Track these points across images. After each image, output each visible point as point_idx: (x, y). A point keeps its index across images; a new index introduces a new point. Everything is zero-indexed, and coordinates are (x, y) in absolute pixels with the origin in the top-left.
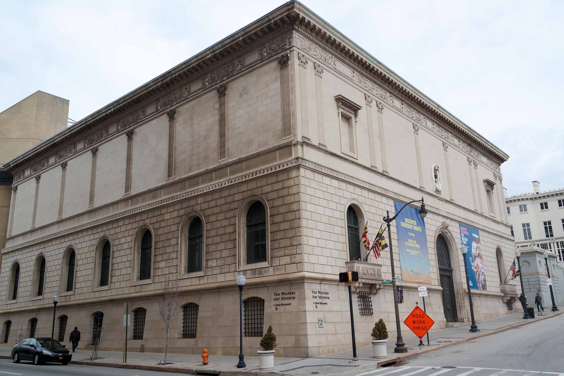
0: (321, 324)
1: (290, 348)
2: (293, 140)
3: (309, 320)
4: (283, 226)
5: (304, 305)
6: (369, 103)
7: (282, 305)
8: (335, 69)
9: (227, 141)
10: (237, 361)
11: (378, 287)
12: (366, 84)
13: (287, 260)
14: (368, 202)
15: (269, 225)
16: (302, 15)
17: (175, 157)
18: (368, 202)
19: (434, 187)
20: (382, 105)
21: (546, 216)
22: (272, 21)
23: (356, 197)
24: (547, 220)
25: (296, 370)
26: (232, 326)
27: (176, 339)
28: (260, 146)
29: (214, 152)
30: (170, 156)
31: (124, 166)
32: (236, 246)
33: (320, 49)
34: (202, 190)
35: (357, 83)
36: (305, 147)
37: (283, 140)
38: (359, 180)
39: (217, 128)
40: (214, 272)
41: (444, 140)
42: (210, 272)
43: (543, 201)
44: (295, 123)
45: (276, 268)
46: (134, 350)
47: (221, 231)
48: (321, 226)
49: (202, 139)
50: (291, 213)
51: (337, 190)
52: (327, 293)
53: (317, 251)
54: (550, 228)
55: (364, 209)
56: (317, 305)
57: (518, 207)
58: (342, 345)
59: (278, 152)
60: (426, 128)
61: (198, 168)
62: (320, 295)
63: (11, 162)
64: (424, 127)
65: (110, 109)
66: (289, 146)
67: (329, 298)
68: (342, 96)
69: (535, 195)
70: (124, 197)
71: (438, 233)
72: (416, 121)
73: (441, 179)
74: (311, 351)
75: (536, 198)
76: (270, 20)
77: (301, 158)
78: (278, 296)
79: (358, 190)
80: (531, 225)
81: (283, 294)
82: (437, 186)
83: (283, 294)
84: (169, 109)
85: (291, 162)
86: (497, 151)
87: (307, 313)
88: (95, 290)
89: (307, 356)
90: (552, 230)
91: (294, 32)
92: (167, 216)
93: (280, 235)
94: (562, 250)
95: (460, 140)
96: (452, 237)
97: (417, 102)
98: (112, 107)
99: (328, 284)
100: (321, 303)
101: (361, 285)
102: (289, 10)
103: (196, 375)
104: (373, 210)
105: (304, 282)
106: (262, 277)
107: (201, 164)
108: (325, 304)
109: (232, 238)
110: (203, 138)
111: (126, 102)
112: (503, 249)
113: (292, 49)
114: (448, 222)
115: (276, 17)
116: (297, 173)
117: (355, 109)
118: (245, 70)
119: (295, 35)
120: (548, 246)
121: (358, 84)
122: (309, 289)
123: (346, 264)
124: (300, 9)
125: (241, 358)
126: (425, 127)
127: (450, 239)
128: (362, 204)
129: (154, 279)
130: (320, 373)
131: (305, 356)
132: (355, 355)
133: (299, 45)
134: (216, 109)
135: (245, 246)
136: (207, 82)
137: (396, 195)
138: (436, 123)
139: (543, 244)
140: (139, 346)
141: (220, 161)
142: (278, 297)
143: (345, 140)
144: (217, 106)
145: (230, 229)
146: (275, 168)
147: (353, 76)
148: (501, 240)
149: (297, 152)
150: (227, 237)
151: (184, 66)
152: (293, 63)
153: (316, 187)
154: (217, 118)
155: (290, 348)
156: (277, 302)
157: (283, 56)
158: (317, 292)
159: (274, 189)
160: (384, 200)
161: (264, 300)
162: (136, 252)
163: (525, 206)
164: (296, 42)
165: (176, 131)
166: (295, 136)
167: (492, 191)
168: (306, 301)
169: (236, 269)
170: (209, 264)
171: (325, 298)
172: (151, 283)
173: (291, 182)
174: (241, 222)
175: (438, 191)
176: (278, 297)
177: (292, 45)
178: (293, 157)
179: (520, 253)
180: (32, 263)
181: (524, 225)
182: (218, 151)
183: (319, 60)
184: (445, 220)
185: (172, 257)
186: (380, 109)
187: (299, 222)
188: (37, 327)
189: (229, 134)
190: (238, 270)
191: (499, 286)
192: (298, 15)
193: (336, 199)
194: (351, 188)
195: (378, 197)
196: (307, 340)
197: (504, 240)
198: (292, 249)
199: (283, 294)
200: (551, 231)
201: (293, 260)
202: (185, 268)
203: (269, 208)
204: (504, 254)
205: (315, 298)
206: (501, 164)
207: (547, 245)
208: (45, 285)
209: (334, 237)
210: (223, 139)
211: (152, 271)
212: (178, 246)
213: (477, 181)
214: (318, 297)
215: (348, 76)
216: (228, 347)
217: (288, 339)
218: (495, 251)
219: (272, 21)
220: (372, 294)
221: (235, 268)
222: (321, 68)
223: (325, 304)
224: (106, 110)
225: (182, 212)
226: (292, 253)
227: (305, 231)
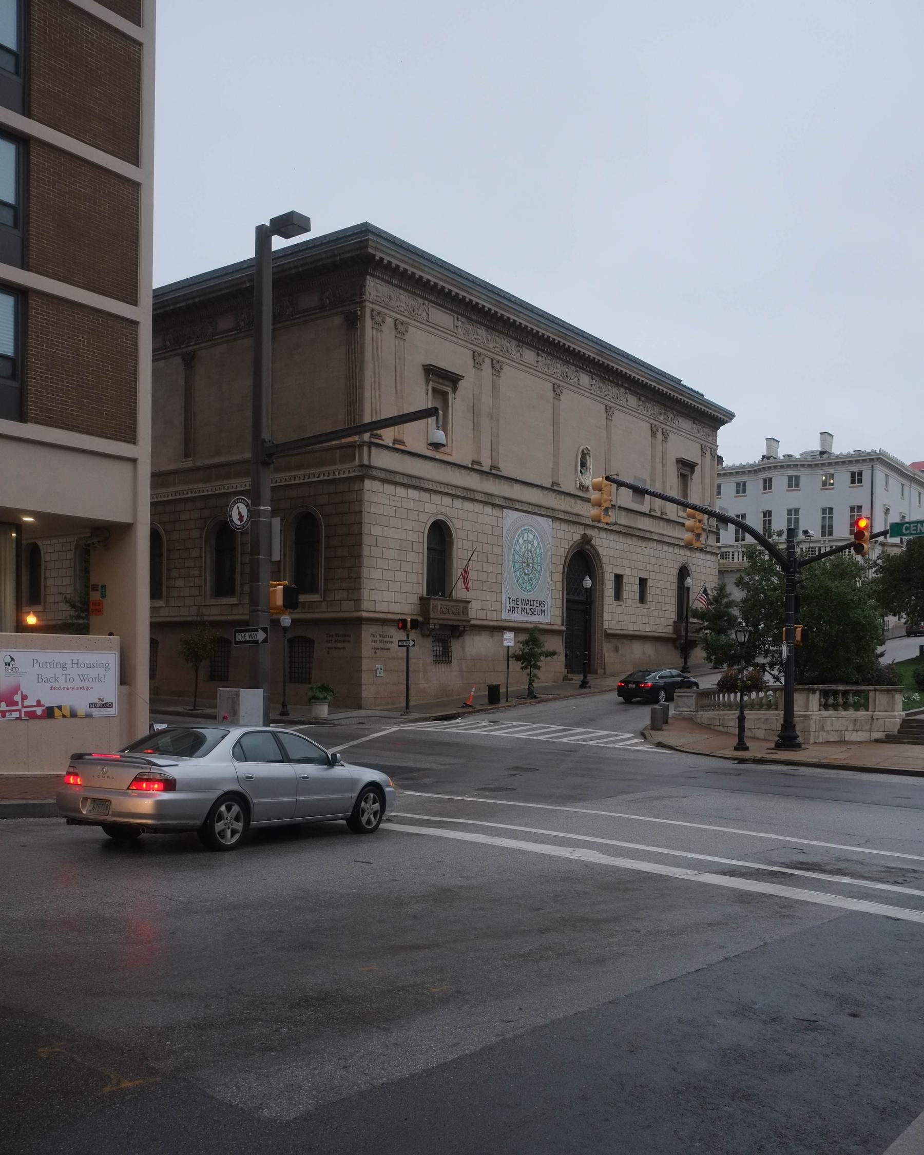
7: (335, 648)
11: (461, 629)
12: (477, 334)
13: (342, 595)
19: (578, 482)
23: (444, 510)
33: (406, 294)
34: (234, 486)
36: (373, 449)
57: (787, 478)
59: (338, 451)
62: (381, 639)
73: (591, 467)
80: (801, 512)
82: (582, 480)
83: (336, 636)
89: (360, 707)
91: (368, 277)
92: (184, 517)
100: (382, 649)
101: (437, 627)
105: (361, 624)
115: (343, 253)
117: (454, 380)
119: (370, 282)
122: (368, 634)
124: (376, 248)
125: (284, 705)
133: (375, 297)
136: (243, 320)
137: (507, 502)
138: (597, 375)
146: (334, 474)
147: (457, 327)
153: (386, 502)
158: (378, 636)
161: (313, 641)
167: (691, 476)
171: (388, 642)
172: (164, 606)
175: (583, 486)
176: (330, 639)
186: (496, 369)
192: (374, 256)
199: (337, 635)
213: (664, 462)
214: (378, 642)
219: (338, 258)
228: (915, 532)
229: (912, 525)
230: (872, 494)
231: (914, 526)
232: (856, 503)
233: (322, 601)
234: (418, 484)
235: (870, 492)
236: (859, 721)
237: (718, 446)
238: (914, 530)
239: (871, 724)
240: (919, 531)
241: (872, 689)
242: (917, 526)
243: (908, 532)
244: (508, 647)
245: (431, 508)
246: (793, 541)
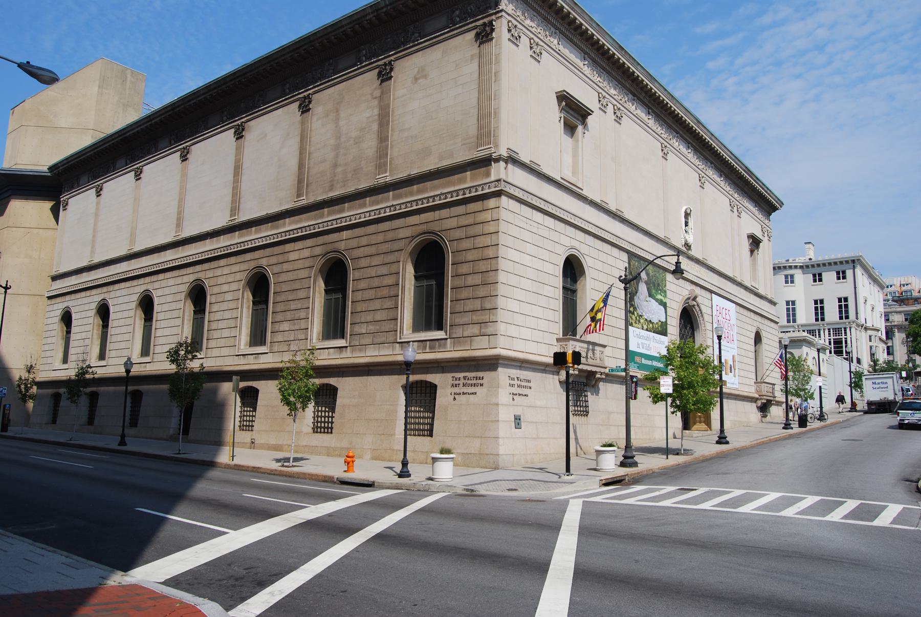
0: (518, 423)
1: (472, 455)
2: (493, 152)
3: (502, 417)
4: (471, 280)
5: (497, 395)
6: (603, 109)
7: (464, 394)
8: (559, 50)
9: (391, 148)
10: (398, 467)
14: (593, 253)
15: (450, 278)
17: (308, 168)
18: (593, 253)
19: (683, 239)
20: (621, 111)
21: (819, 291)
24: (818, 297)
25: (485, 484)
26: (386, 420)
28: (441, 158)
29: (370, 163)
30: (301, 166)
31: (230, 177)
32: (398, 305)
35: (589, 75)
36: (510, 166)
37: (478, 151)
38: (583, 220)
39: (375, 127)
40: (364, 342)
41: (700, 172)
42: (356, 340)
43: (817, 270)
44: (498, 127)
45: (457, 340)
46: (243, 445)
47: (376, 282)
48: (526, 284)
49: (352, 142)
50: (485, 262)
51: (552, 232)
52: (529, 381)
53: (519, 319)
54: (822, 308)
55: (588, 263)
56: (515, 397)
58: (544, 454)
60: (679, 152)
61: (344, 185)
62: (519, 383)
64: (676, 149)
66: (485, 162)
67: (530, 388)
68: (567, 93)
69: (808, 262)
70: (228, 224)
71: (683, 306)
72: (666, 140)
73: (692, 228)
74: (502, 461)
75: (807, 267)
77: (504, 181)
78: (458, 381)
79: (580, 235)
80: (797, 303)
81: (465, 379)
82: (687, 238)
84: (481, 22)
85: (488, 185)
86: (769, 194)
87: (500, 407)
88: (405, 338)
90: (823, 312)
93: (464, 294)
94: (834, 339)
97: (669, 112)
100: (520, 395)
103: (338, 484)
104: (598, 265)
106: (435, 353)
107: (348, 180)
108: (525, 395)
109: (392, 293)
110: (354, 141)
112: (763, 334)
113: (500, 14)
114: (698, 290)
116: (497, 202)
120: (832, 332)
121: (590, 77)
123: (557, 341)
126: (677, 151)
128: (584, 255)
129: (271, 346)
130: (519, 489)
131: (494, 466)
132: (568, 469)
134: (376, 98)
136: (364, 56)
138: (692, 146)
139: (836, 329)
140: (249, 441)
141: (378, 177)
142: (457, 382)
143: (568, 159)
144: (378, 93)
145: (389, 281)
148: (763, 322)
149: (498, 172)
150: (384, 292)
152: (500, 37)
155: (472, 455)
156: (457, 390)
157: (485, 24)
158: (516, 379)
159: (461, 224)
160: (615, 252)
163: (792, 276)
165: (313, 129)
166: (497, 146)
168: (500, 390)
169: (396, 339)
173: (487, 216)
174: (137, 315)
176: (457, 382)
177: (499, 8)
178: (493, 178)
179: (789, 340)
181: (788, 303)
182: (375, 163)
183: (538, 35)
184: (694, 287)
185: (299, 317)
187: (496, 276)
188: (99, 404)
189: (394, 136)
190: (399, 340)
191: (753, 384)
193: (549, 245)
194: (571, 231)
196: (498, 444)
197: (766, 322)
198: (482, 315)
200: (822, 314)
201: (483, 330)
202: (319, 334)
203: (451, 253)
204: (764, 340)
205: (512, 386)
206: (772, 214)
207: (833, 334)
208: (109, 346)
209: (543, 301)
210: (384, 144)
211: (205, 341)
212: (309, 300)
214: (516, 386)
216: (380, 449)
217: (469, 442)
218: (753, 336)
220: (589, 386)
221: (395, 337)
222: (540, 47)
223: (525, 395)
225: (318, 251)
226: (483, 320)
227: (501, 290)
230: (855, 288)
232: (843, 295)
233: (446, 339)
235: (853, 287)
245: (567, 242)
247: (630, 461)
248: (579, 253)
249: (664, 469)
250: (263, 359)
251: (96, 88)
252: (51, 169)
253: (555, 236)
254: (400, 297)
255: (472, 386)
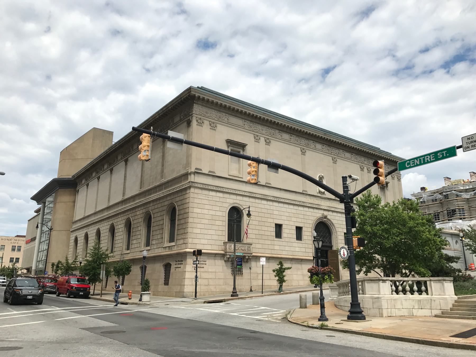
5: (185, 268)
7: (178, 267)
16: (197, 95)
22: (183, 99)
27: (136, 286)
63: (75, 174)
65: (117, 145)
66: (186, 175)
76: (181, 98)
92: (138, 213)
95: (352, 153)
96: (332, 224)
98: (117, 144)
99: (206, 256)
102: (189, 92)
111: (123, 142)
115: (184, 96)
118: (174, 126)
127: (331, 225)
135: (169, 232)
138: (325, 144)
151: (147, 122)
154: (161, 154)
162: (125, 234)
164: (196, 111)
168: (187, 265)
170: (152, 242)
175: (321, 192)
180: (94, 234)
183: (215, 119)
190: (163, 247)
195: (259, 201)
215: (241, 125)
219: (183, 99)
224: (115, 146)
228: (414, 165)
229: (411, 161)
231: (412, 162)
233: (175, 245)
234: (222, 190)
236: (421, 302)
237: (401, 175)
238: (412, 164)
239: (431, 304)
240: (416, 164)
241: (428, 279)
242: (414, 162)
243: (409, 165)
244: (263, 265)
245: (232, 201)
246: (346, 184)
247: (235, 294)
248: (239, 205)
249: (31, 271)
250: (129, 255)
251: (91, 141)
252: (73, 176)
253: (224, 200)
254: (164, 229)
255: (202, 264)
